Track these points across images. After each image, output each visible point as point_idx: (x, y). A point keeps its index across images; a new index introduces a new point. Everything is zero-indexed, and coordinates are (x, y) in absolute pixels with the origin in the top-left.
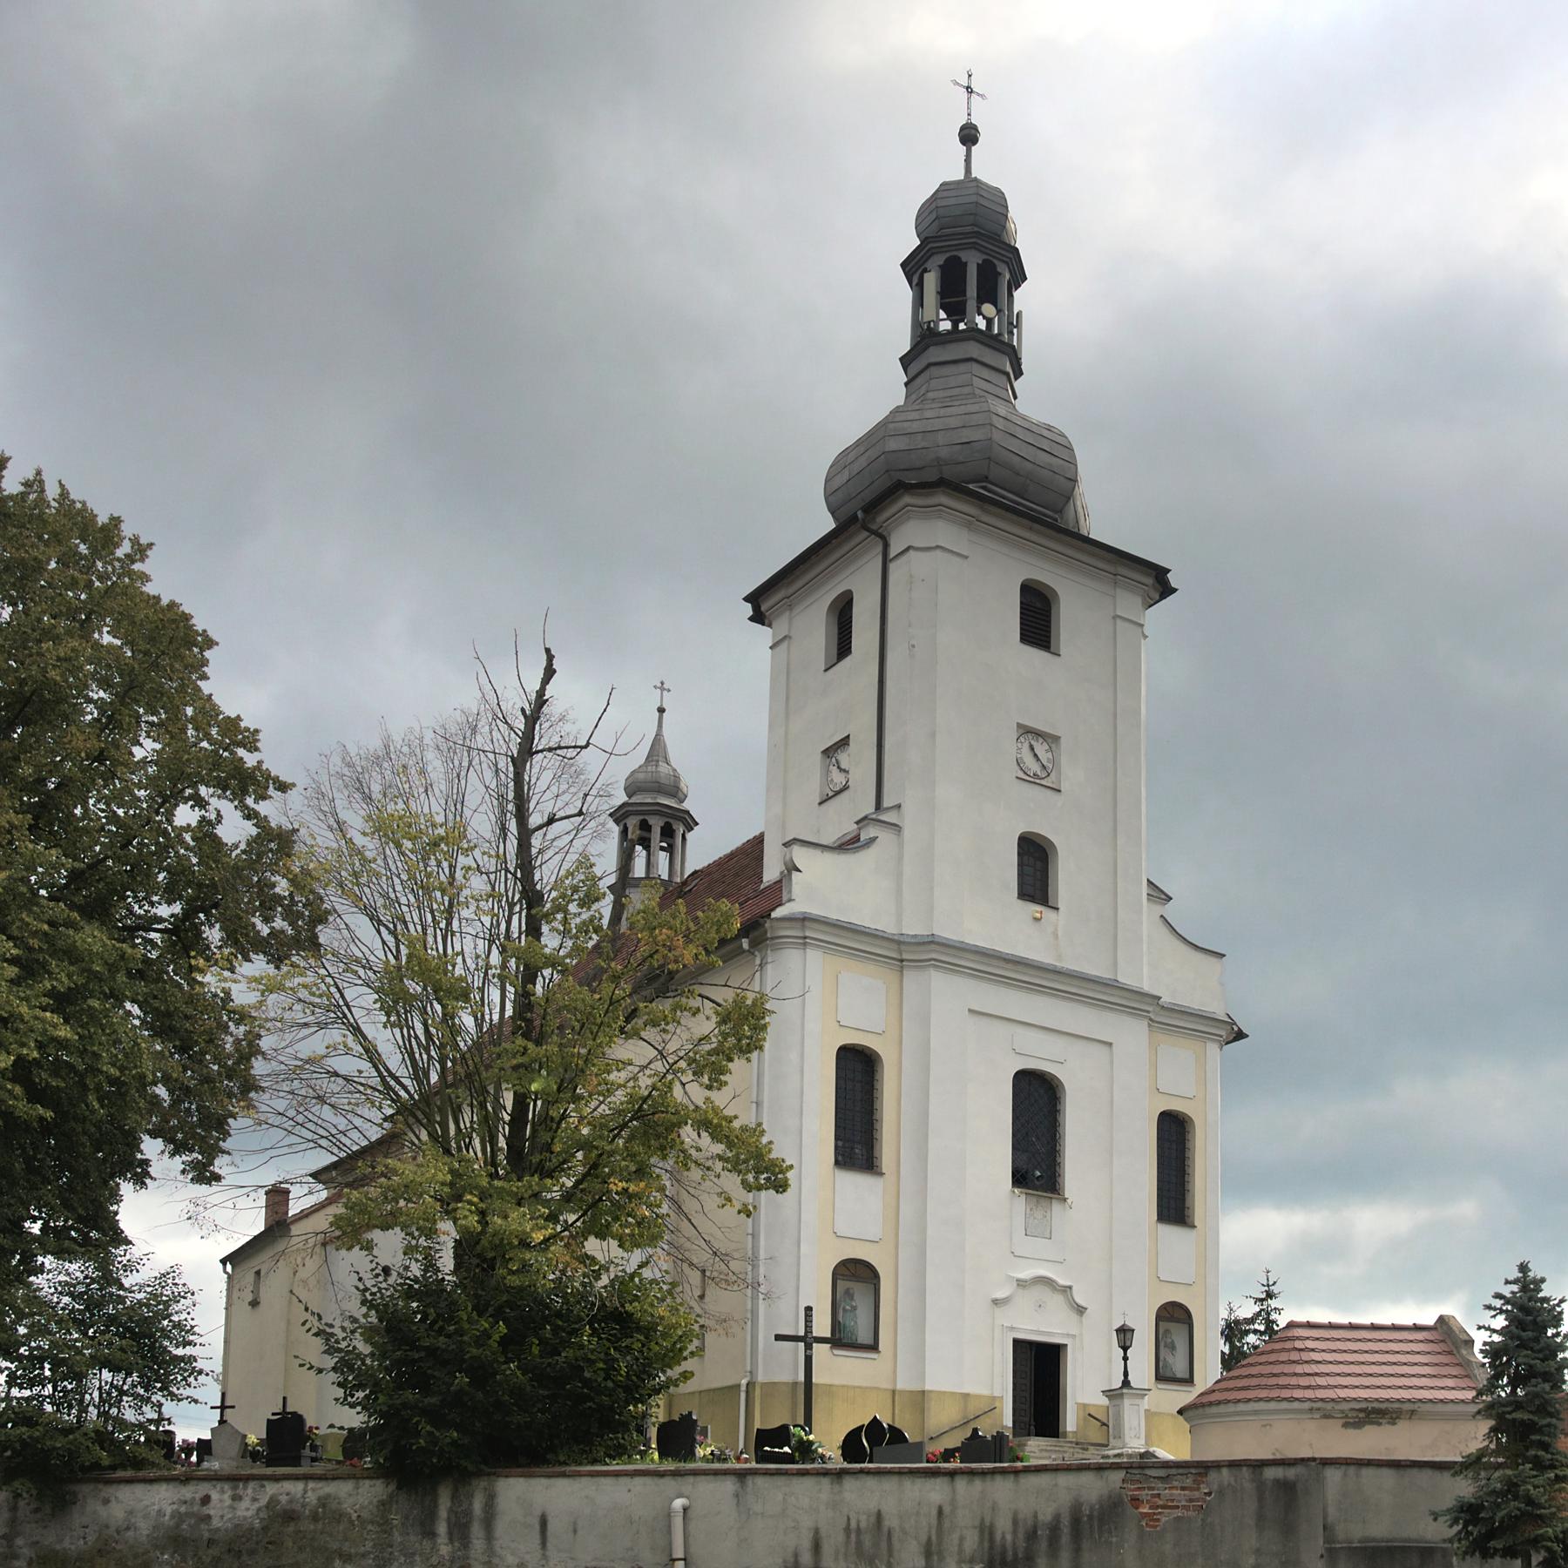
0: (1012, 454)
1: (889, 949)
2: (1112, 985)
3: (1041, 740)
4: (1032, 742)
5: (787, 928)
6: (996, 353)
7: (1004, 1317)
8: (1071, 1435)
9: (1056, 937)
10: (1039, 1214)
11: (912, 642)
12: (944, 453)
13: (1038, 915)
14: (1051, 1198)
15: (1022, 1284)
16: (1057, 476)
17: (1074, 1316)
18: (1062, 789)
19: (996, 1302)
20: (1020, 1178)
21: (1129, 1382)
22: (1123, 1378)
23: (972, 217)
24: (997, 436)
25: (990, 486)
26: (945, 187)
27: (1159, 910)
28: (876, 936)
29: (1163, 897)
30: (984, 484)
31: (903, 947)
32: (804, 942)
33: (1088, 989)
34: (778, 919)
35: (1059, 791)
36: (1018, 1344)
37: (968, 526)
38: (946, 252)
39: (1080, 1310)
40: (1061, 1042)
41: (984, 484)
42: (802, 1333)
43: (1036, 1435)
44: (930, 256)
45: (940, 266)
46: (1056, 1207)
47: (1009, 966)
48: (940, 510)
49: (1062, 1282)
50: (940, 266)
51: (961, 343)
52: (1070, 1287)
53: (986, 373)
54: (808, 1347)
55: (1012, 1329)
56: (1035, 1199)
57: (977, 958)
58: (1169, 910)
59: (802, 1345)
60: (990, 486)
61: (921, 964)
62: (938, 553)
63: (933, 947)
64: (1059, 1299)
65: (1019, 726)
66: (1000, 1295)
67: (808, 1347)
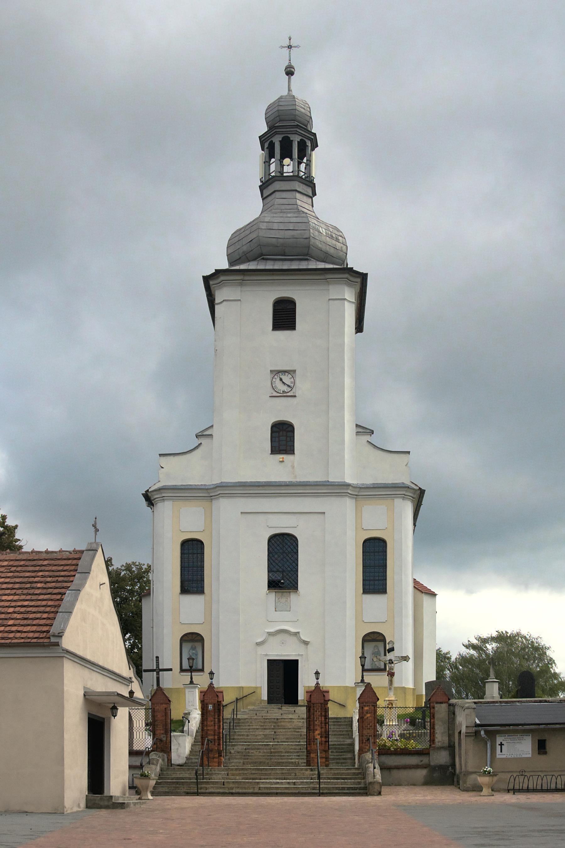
0: (272, 239)
1: (204, 493)
2: (326, 484)
3: (287, 374)
4: (281, 377)
5: (212, 492)
6: (289, 182)
7: (261, 651)
8: (300, 701)
9: (293, 467)
10: (283, 600)
11: (216, 349)
12: (245, 248)
13: (281, 460)
14: (290, 592)
15: (270, 634)
16: (299, 239)
17: (303, 646)
18: (297, 395)
19: (258, 644)
20: (273, 585)
21: (364, 680)
22: (361, 678)
23: (278, 117)
24: (262, 234)
25: (265, 257)
26: (281, 97)
27: (365, 438)
28: (287, 485)
29: (368, 431)
30: (262, 257)
31: (209, 491)
32: (163, 499)
33: (291, 490)
34: (150, 492)
35: (295, 396)
36: (271, 663)
37: (241, 285)
38: (268, 140)
39: (306, 643)
40: (293, 518)
41: (262, 257)
42: (155, 668)
43: (285, 704)
44: (275, 135)
45: (280, 141)
46: (293, 596)
47: (261, 488)
48: (224, 283)
49: (293, 630)
50: (280, 141)
51: (272, 184)
52: (298, 633)
53: (284, 195)
54: (158, 674)
55: (266, 655)
56: (280, 594)
57: (241, 488)
58: (373, 439)
59: (155, 673)
60: (265, 257)
61: (218, 496)
62: (225, 303)
63: (218, 489)
64: (294, 639)
65: (271, 371)
66: (259, 640)
67: (158, 674)
